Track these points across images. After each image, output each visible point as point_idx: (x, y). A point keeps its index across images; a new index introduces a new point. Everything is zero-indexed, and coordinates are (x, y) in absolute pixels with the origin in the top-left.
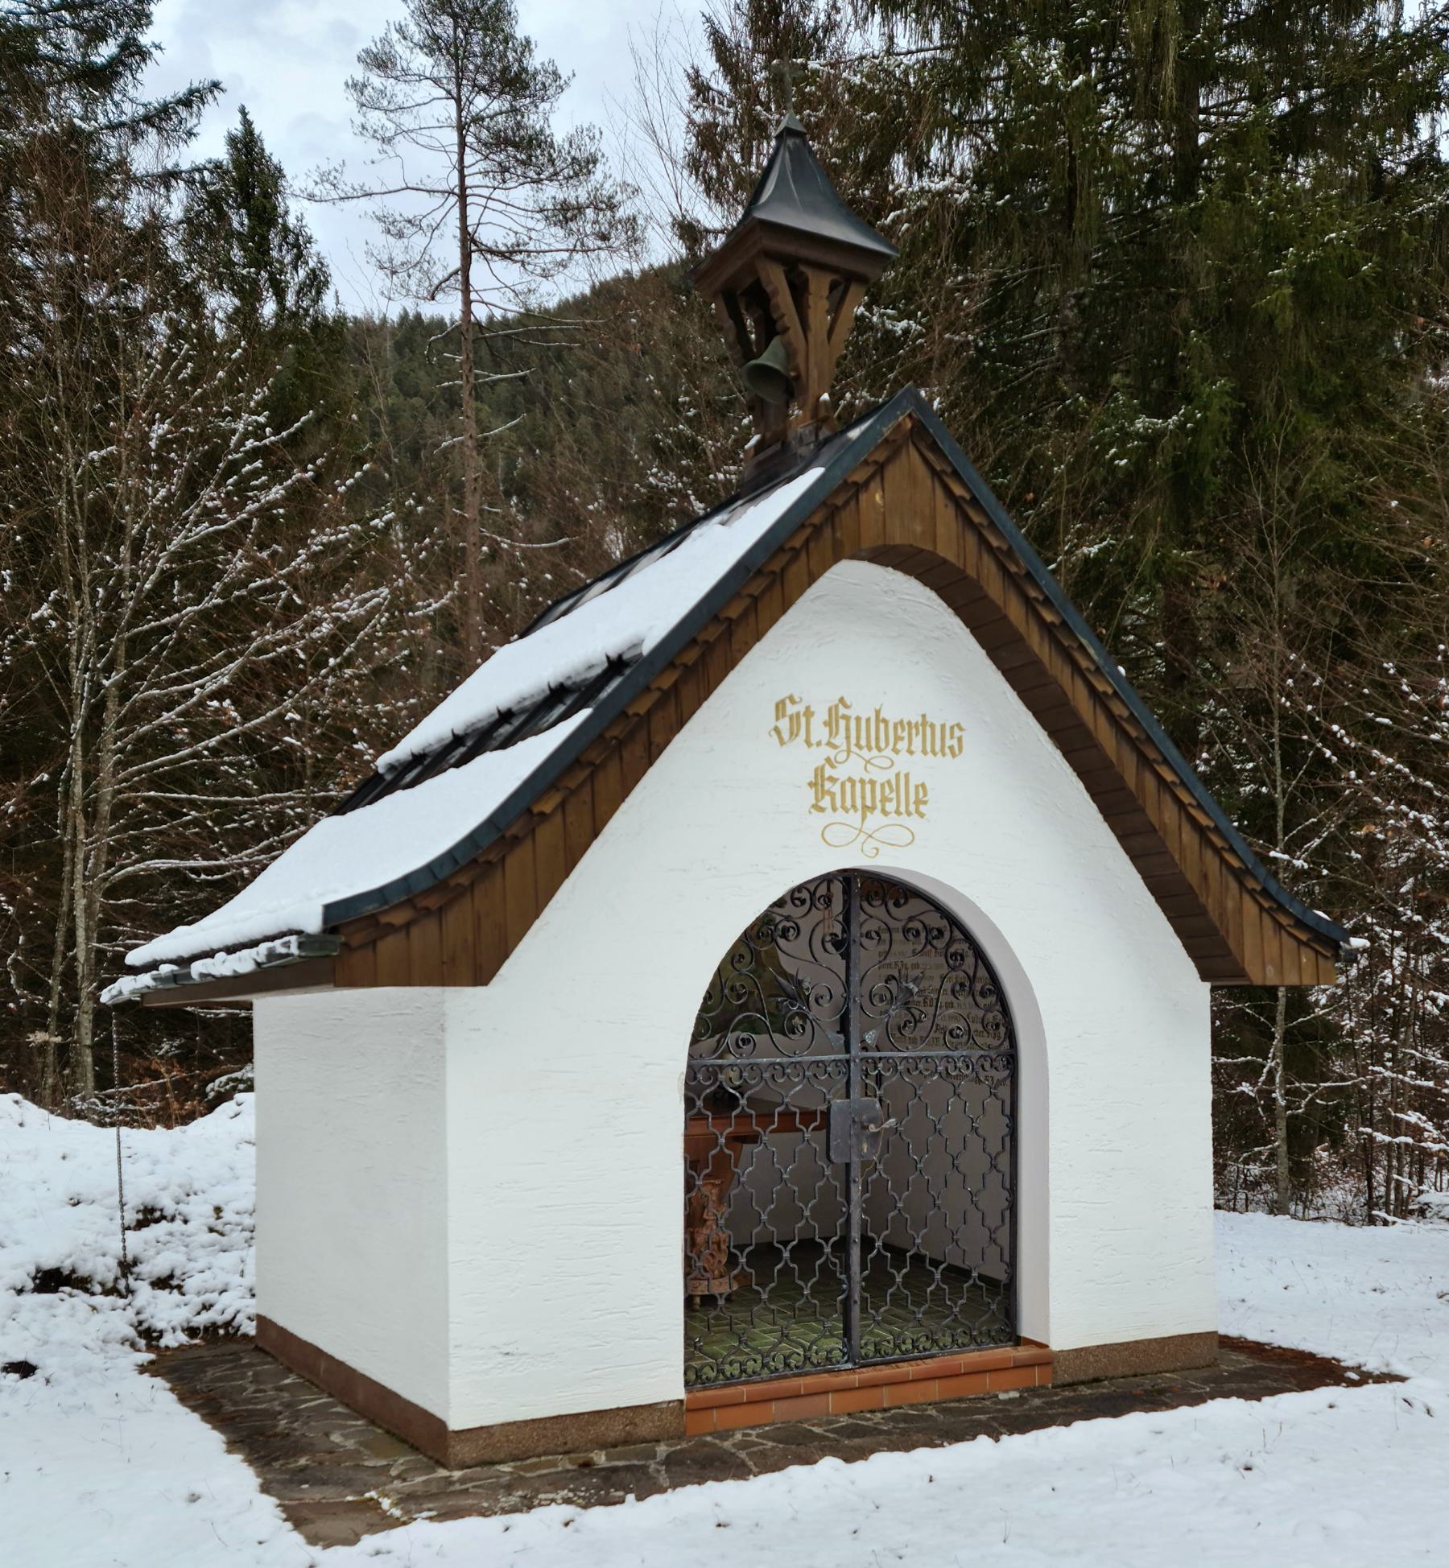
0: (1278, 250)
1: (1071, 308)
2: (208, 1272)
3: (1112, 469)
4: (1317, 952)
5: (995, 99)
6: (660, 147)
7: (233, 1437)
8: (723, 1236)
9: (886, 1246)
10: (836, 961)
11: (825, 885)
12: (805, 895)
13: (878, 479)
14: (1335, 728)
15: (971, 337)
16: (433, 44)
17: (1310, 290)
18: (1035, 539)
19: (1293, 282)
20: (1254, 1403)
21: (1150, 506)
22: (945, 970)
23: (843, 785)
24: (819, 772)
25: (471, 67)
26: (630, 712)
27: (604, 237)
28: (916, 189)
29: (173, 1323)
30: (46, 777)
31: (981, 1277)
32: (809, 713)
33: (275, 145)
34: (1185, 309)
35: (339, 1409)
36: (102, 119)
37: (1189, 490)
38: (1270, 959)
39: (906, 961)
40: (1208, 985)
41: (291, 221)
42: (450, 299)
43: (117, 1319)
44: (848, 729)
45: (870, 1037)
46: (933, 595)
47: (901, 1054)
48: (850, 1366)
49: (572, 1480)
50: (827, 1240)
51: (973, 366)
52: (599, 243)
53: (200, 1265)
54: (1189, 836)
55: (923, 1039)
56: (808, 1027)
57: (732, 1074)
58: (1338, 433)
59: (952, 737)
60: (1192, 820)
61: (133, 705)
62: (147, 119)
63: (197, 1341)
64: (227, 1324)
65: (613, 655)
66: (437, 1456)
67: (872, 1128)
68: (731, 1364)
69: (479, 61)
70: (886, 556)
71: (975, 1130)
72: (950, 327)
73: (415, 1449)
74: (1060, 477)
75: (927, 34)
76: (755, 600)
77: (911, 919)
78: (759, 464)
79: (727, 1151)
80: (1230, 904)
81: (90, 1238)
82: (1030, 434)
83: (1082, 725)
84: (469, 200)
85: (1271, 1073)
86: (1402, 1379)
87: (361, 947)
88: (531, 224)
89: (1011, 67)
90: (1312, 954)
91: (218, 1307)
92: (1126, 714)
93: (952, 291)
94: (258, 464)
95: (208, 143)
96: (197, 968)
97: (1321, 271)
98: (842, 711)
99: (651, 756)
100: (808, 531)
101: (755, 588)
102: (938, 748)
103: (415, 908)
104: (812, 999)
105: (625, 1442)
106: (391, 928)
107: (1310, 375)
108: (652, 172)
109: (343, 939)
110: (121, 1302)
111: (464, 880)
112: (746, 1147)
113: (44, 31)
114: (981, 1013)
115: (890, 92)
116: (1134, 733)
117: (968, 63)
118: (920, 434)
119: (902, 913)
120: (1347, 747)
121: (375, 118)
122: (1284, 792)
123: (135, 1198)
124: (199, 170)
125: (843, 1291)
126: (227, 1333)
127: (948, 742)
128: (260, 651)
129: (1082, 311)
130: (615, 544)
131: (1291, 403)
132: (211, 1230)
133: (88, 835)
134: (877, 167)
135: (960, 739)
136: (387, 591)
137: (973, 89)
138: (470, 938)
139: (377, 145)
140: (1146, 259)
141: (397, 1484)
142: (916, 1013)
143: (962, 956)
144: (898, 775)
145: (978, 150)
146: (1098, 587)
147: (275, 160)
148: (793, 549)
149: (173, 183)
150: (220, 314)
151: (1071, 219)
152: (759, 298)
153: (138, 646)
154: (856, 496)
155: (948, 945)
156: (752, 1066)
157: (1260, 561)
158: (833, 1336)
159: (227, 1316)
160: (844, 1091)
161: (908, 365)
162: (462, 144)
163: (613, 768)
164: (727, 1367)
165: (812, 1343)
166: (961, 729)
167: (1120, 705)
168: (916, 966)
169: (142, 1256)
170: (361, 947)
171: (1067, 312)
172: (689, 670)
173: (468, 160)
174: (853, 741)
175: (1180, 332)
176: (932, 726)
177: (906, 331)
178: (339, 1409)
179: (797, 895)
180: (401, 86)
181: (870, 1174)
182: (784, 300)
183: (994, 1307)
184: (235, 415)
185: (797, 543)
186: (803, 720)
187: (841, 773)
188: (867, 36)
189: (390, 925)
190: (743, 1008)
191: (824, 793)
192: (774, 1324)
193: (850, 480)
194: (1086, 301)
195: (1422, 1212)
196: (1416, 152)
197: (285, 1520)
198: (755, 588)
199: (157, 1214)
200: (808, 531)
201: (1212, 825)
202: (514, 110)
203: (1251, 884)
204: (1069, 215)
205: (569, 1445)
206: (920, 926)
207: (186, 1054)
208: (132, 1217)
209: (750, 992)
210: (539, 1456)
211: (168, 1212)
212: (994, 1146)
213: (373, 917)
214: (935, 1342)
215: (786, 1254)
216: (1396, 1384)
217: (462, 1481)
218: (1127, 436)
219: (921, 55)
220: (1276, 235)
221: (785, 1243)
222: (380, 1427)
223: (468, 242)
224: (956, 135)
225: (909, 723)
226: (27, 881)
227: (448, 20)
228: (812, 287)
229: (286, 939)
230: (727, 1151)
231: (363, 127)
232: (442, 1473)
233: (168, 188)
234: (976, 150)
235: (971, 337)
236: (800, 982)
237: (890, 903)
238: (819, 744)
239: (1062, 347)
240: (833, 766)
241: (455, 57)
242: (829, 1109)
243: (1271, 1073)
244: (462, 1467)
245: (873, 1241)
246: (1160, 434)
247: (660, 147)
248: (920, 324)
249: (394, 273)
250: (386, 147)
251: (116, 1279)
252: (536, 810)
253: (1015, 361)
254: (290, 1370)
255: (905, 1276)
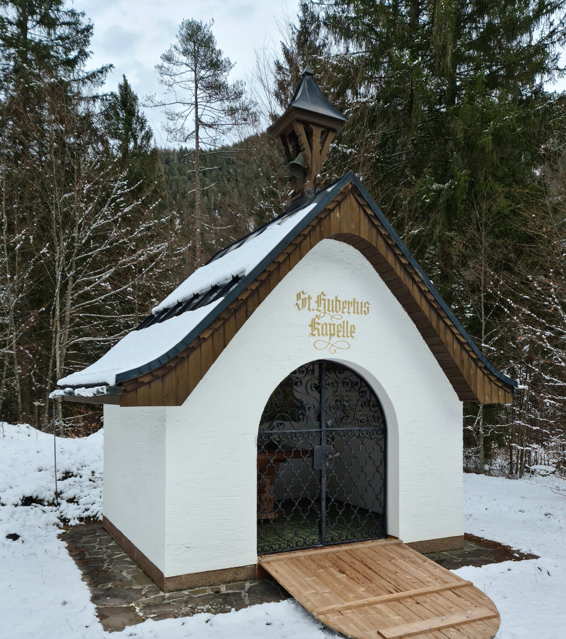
0: (486, 122)
1: (410, 144)
2: (88, 496)
3: (423, 202)
4: (505, 390)
5: (384, 69)
6: (265, 87)
7: (86, 571)
8: (272, 497)
9: (336, 501)
10: (316, 394)
11: (312, 365)
12: (304, 369)
13: (338, 207)
14: (509, 300)
15: (374, 155)
16: (185, 52)
17: (498, 138)
18: (396, 228)
19: (492, 134)
20: (479, 568)
21: (438, 216)
22: (359, 398)
23: (322, 326)
24: (313, 320)
25: (200, 60)
26: (239, 298)
27: (245, 120)
28: (355, 101)
29: (74, 516)
30: (44, 309)
31: (372, 512)
32: (310, 298)
33: (135, 88)
34: (451, 144)
35: (128, 559)
36: (72, 77)
37: (452, 211)
38: (487, 393)
39: (343, 394)
40: (462, 402)
41: (140, 114)
42: (191, 141)
43: (52, 515)
44: (325, 304)
45: (329, 423)
46: (359, 252)
47: (341, 429)
48: (321, 545)
49: (212, 599)
50: (312, 498)
51: (375, 166)
52: (243, 122)
53: (85, 494)
54: (456, 346)
55: (350, 423)
56: (305, 418)
57: (276, 436)
58: (507, 189)
59: (365, 307)
60: (458, 340)
61: (77, 284)
62: (88, 78)
63: (82, 523)
64: (94, 516)
65: (235, 275)
66: (161, 586)
67: (330, 456)
68: (275, 545)
69: (203, 58)
70: (341, 237)
71: (370, 457)
72: (367, 151)
73: (153, 581)
74: (406, 205)
75: (361, 46)
76: (289, 255)
77: (345, 378)
78: (293, 201)
79: (274, 465)
80: (472, 372)
81: (44, 484)
82: (394, 190)
83: (415, 303)
84: (199, 107)
85: (478, 422)
86: (536, 557)
87: (132, 391)
88: (220, 115)
89: (391, 58)
90: (503, 391)
91: (91, 510)
92: (433, 299)
93: (368, 138)
94: (122, 199)
95: (110, 86)
96: (77, 392)
97: (503, 130)
98: (323, 297)
99: (247, 315)
100: (310, 228)
101: (289, 250)
102: (359, 311)
103: (152, 375)
104: (307, 408)
105: (234, 581)
106: (143, 384)
107: (497, 168)
108: (261, 95)
109: (124, 388)
110: (55, 508)
111: (172, 364)
112: (281, 464)
113: (52, 47)
114: (372, 414)
115: (346, 67)
116: (436, 306)
117: (375, 56)
118: (355, 190)
119: (342, 376)
120: (513, 307)
121: (166, 78)
122: (485, 320)
123: (62, 468)
124: (105, 95)
125: (319, 518)
126: (94, 520)
127: (364, 309)
128: (121, 265)
129: (415, 145)
130: (252, 226)
131: (490, 178)
132: (90, 480)
133: (61, 328)
134: (341, 94)
135: (368, 308)
136: (167, 244)
137: (377, 66)
138: (175, 387)
139: (167, 87)
140: (439, 127)
141: (144, 599)
142: (348, 414)
143: (365, 392)
144: (344, 322)
145: (378, 87)
146: (418, 245)
147: (135, 93)
148: (304, 235)
149: (96, 100)
150: (115, 147)
151: (411, 112)
152: (294, 137)
153: (78, 264)
154: (329, 214)
155: (360, 388)
156: (283, 434)
157: (477, 236)
158: (315, 534)
159: (94, 513)
160: (319, 443)
161: (351, 165)
162: (197, 87)
163: (232, 321)
164: (274, 546)
165: (307, 537)
166: (369, 304)
167: (430, 295)
168: (347, 396)
169: (64, 491)
170: (132, 391)
171: (409, 146)
172: (263, 282)
173: (198, 92)
174: (327, 309)
175: (450, 153)
176: (358, 303)
177: (351, 153)
178: (128, 559)
179: (301, 369)
180: (175, 67)
181: (329, 474)
182: (303, 138)
183: (377, 523)
184: (116, 180)
185: (306, 232)
186: (307, 301)
187: (322, 321)
188: (339, 48)
189: (143, 382)
190: (280, 412)
191: (315, 329)
192: (292, 530)
193: (327, 208)
194: (416, 142)
195: (533, 472)
196: (535, 88)
197: (97, 616)
198: (289, 250)
199: (71, 474)
200: (310, 228)
201: (465, 342)
202: (214, 75)
203: (480, 364)
204: (410, 111)
205: (212, 583)
206: (349, 381)
207: (83, 416)
208: (60, 475)
209: (283, 405)
210: (200, 587)
211: (75, 474)
212: (378, 463)
213: (136, 380)
214: (355, 537)
215: (297, 504)
216: (534, 560)
217: (169, 598)
218: (429, 191)
219: (358, 55)
220: (486, 117)
221: (296, 500)
222: (141, 569)
223: (198, 122)
224: (370, 82)
225: (348, 302)
226: (39, 345)
227: (192, 44)
228: (314, 133)
229: (103, 387)
230: (274, 465)
231: (162, 81)
232: (162, 594)
233: (94, 101)
234: (377, 88)
235: (374, 155)
236: (302, 402)
237: (337, 373)
238: (313, 310)
239: (407, 158)
240: (319, 319)
241: (195, 57)
242: (313, 449)
243: (478, 422)
244: (170, 591)
245: (330, 499)
246: (442, 190)
247: (265, 87)
248: (356, 150)
249: (171, 132)
250: (170, 88)
251: (54, 499)
252: (201, 337)
253: (388, 164)
254: (113, 539)
255: (343, 512)
